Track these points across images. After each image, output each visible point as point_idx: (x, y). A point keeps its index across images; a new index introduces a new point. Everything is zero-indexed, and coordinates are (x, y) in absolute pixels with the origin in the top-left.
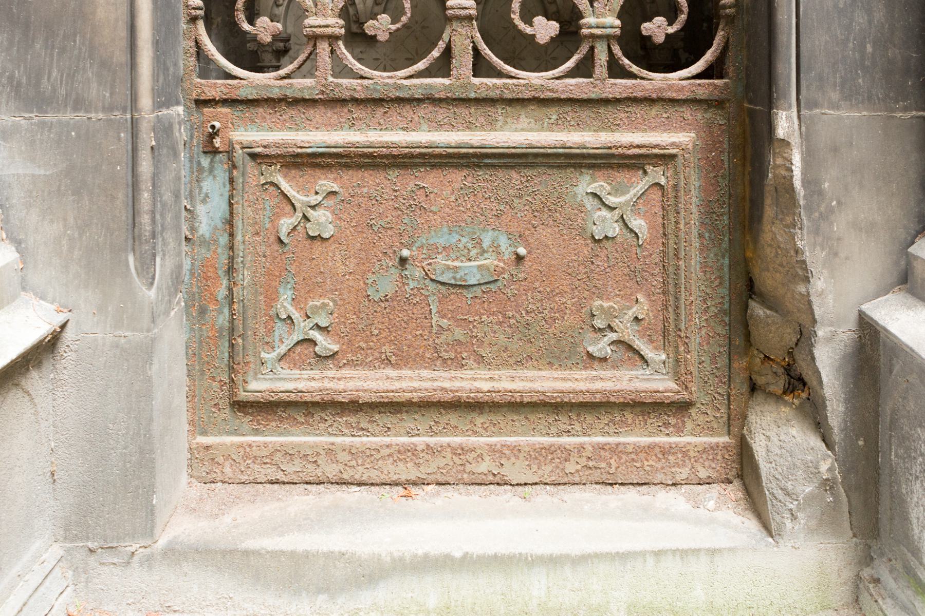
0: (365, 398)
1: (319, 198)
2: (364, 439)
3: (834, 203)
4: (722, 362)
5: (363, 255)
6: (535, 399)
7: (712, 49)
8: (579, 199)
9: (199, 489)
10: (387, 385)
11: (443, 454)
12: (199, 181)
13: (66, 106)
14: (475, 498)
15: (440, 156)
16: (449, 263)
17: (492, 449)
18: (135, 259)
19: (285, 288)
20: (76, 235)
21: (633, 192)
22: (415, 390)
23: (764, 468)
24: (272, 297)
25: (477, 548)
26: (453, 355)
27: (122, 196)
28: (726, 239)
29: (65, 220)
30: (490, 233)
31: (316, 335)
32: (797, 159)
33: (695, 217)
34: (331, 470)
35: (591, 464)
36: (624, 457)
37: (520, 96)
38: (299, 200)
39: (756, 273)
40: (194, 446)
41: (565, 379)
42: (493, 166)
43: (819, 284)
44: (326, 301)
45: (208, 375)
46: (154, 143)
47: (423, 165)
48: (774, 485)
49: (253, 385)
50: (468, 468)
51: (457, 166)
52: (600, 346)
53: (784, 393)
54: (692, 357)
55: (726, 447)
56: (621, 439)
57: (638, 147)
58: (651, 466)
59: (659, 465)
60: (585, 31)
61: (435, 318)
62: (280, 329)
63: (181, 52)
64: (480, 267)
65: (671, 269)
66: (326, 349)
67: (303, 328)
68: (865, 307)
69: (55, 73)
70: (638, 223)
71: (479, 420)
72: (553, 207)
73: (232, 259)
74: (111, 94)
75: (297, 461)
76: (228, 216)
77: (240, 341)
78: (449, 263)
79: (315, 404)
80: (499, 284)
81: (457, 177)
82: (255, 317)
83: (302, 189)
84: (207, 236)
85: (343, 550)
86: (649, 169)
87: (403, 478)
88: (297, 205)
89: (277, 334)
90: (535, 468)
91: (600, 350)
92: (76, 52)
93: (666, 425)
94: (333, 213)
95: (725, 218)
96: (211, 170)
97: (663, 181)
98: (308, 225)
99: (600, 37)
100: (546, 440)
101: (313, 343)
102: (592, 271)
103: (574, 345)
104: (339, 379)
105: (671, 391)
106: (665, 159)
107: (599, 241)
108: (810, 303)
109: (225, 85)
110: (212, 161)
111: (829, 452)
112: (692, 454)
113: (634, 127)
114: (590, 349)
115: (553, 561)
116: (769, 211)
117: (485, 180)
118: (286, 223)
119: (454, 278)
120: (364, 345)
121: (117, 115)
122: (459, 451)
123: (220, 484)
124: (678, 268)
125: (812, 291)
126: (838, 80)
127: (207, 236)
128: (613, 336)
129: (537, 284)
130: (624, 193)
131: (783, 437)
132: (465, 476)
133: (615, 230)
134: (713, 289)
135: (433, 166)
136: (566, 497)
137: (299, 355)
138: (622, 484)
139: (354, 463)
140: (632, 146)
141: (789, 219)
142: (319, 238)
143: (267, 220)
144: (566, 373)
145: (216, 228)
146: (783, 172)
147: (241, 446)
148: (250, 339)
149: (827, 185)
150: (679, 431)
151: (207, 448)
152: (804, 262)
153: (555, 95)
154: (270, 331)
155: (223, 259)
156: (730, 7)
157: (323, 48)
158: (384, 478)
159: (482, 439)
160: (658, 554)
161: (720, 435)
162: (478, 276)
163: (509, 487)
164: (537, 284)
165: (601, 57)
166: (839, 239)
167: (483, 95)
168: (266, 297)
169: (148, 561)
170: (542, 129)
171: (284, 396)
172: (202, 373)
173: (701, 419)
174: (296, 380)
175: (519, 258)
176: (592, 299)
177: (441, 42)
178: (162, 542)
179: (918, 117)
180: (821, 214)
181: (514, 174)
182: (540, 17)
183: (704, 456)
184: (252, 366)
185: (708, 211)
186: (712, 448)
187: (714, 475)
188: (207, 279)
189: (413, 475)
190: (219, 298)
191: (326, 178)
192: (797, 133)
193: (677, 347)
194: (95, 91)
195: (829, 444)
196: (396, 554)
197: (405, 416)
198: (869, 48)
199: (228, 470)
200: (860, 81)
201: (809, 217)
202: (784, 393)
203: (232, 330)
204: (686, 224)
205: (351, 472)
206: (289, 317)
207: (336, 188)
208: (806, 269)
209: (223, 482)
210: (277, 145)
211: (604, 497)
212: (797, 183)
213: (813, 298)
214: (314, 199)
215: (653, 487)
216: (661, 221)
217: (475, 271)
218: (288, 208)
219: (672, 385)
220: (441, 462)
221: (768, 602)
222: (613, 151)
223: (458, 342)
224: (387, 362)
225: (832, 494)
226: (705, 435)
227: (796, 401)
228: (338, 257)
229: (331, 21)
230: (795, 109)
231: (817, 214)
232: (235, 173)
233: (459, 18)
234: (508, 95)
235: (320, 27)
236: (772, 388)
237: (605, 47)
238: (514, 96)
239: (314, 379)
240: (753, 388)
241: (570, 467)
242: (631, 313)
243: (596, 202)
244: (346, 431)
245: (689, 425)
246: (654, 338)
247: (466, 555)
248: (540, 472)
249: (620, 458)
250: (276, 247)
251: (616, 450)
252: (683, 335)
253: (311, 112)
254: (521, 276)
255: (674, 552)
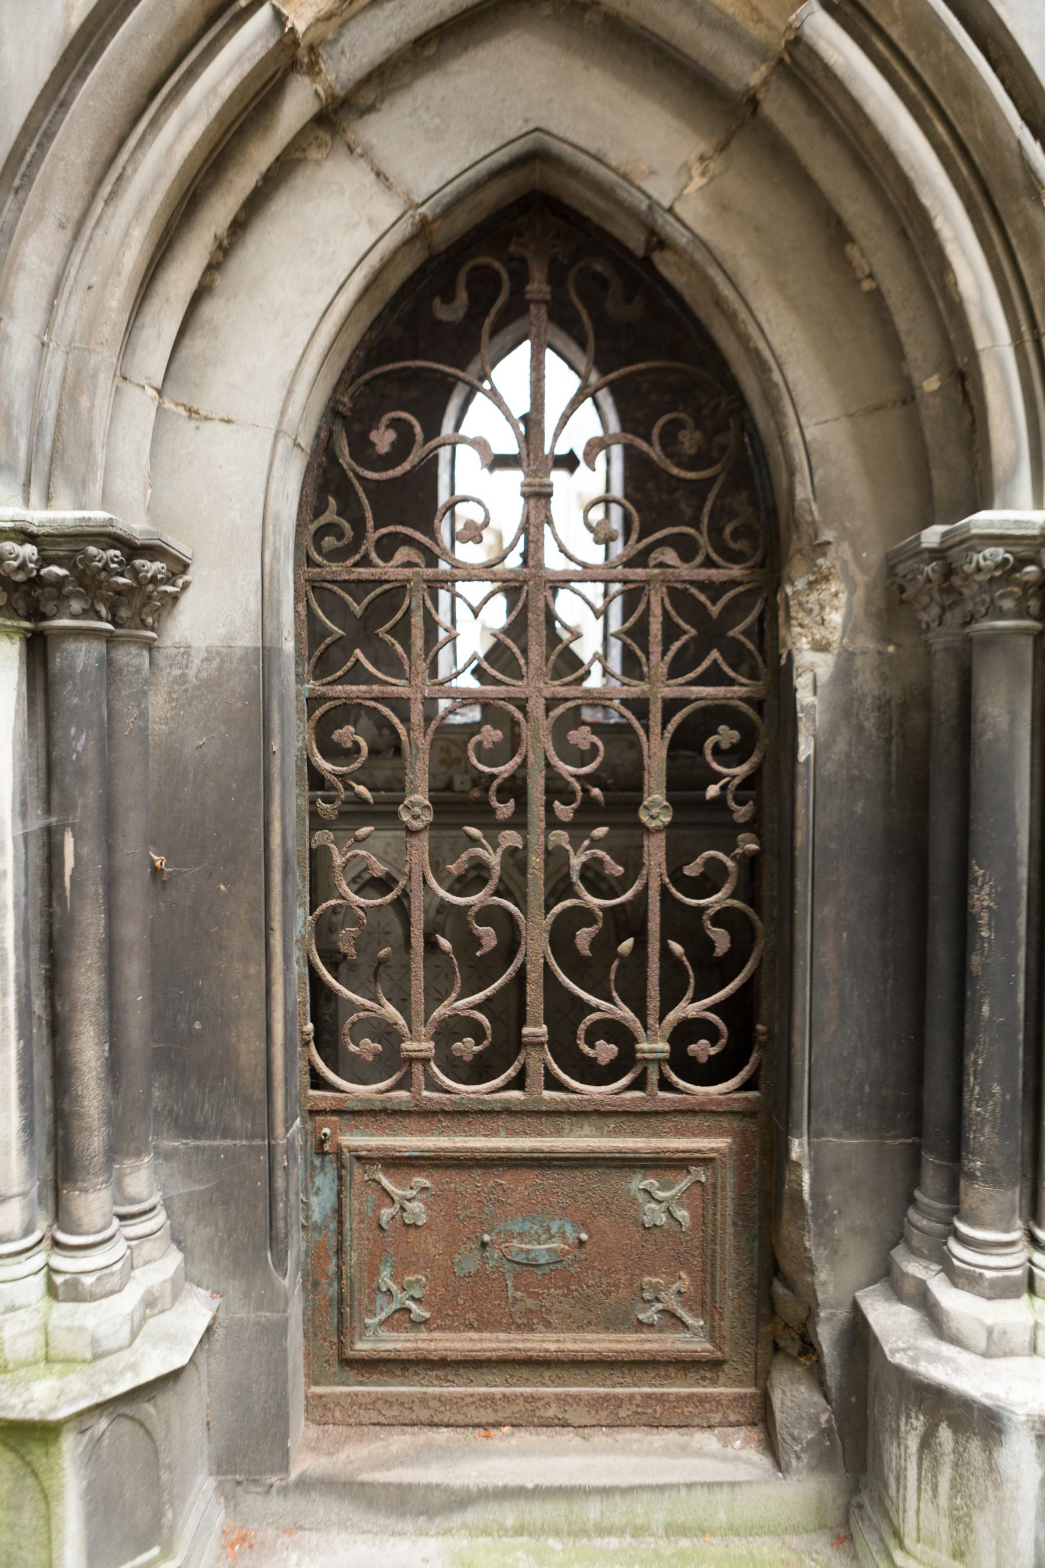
0: (452, 1356)
1: (414, 1193)
2: (451, 1389)
3: (836, 1212)
4: (751, 1326)
5: (451, 1239)
6: (594, 1358)
7: (747, 1068)
8: (632, 1194)
9: (314, 1431)
10: (468, 1346)
11: (517, 1401)
12: (312, 1177)
13: (216, 1134)
14: (544, 1438)
15: (516, 1159)
16: (523, 1246)
17: (558, 1398)
18: (272, 1256)
19: (385, 1266)
20: (225, 1236)
21: (678, 1187)
22: (494, 1350)
23: (778, 1415)
24: (375, 1273)
25: (545, 1481)
26: (525, 1321)
27: (262, 1206)
28: (756, 1226)
29: (216, 1224)
30: (558, 1222)
31: (413, 1306)
32: (806, 1177)
33: (730, 1210)
34: (424, 1415)
35: (640, 1410)
36: (667, 1405)
37: (584, 1109)
38: (397, 1195)
39: (778, 1256)
40: (309, 1395)
41: (619, 1341)
42: (561, 1167)
43: (822, 1275)
44: (420, 1277)
45: (320, 1336)
46: (286, 1164)
47: (502, 1166)
48: (784, 1432)
49: (359, 1346)
50: (538, 1413)
51: (530, 1167)
52: (648, 1314)
53: (800, 1354)
54: (726, 1324)
55: (753, 1396)
56: (665, 1390)
57: (683, 1152)
58: (690, 1412)
59: (696, 1412)
60: (639, 1055)
61: (511, 1291)
62: (381, 1299)
63: (298, 1071)
64: (548, 1250)
65: (709, 1252)
66: (419, 1316)
67: (401, 1298)
68: (857, 1294)
69: (207, 1107)
70: (682, 1214)
71: (547, 1374)
72: (609, 1201)
73: (340, 1243)
74: (253, 1125)
75: (395, 1408)
76: (336, 1206)
77: (348, 1310)
78: (523, 1246)
79: (410, 1362)
80: (565, 1263)
81: (532, 1177)
82: (360, 1290)
83: (399, 1185)
84: (319, 1222)
85: (439, 1482)
86: (693, 1169)
87: (484, 1421)
88: (396, 1198)
89: (378, 1304)
90: (593, 1413)
91: (648, 1318)
92: (223, 1091)
93: (704, 1378)
94: (425, 1204)
95: (756, 1208)
96: (322, 1168)
97: (703, 1179)
98: (405, 1215)
99: (652, 1060)
100: (602, 1390)
101: (409, 1311)
102: (643, 1253)
103: (627, 1313)
104: (431, 1341)
105: (707, 1351)
106: (705, 1161)
107: (649, 1228)
108: (814, 1291)
109: (333, 1098)
110: (323, 1161)
111: (829, 1407)
112: (724, 1402)
113: (680, 1133)
114: (640, 1317)
115: (605, 1492)
116: (786, 1214)
117: (554, 1179)
118: (386, 1213)
119: (527, 1259)
120: (451, 1313)
121: (258, 1142)
122: (530, 1400)
123: (331, 1426)
124: (714, 1251)
125: (816, 1281)
126: (841, 1114)
127: (319, 1222)
128: (660, 1306)
129: (596, 1264)
130: (670, 1189)
131: (794, 1393)
132: (535, 1420)
133: (663, 1219)
134: (745, 1267)
135: (510, 1167)
136: (618, 1438)
137: (397, 1320)
138: (666, 1426)
139: (443, 1409)
140: (677, 1151)
141: (800, 1223)
142: (415, 1226)
143: (370, 1210)
144: (619, 1336)
145: (326, 1216)
146: (796, 1186)
147: (348, 1395)
148: (356, 1308)
149: (830, 1197)
150: (714, 1383)
151: (320, 1397)
152: (810, 1258)
153: (613, 1109)
154: (372, 1301)
155: (333, 1242)
156: (763, 1035)
157: (418, 1069)
158: (467, 1421)
159: (550, 1390)
160: (690, 1486)
161: (749, 1387)
162: (547, 1257)
163: (572, 1429)
164: (596, 1264)
165: (653, 1077)
166: (839, 1240)
167: (552, 1109)
168: (369, 1273)
169: (284, 1491)
170: (602, 1136)
171: (384, 1355)
172: (315, 1335)
173: (733, 1374)
174: (395, 1341)
175: (581, 1243)
176: (641, 1275)
177: (516, 1063)
178: (294, 1475)
179: (905, 1144)
180: (825, 1220)
181: (577, 1173)
182: (602, 1041)
183: (735, 1404)
184: (358, 1329)
185: (741, 1202)
186: (741, 1397)
187: (742, 1419)
188: (319, 1258)
189: (492, 1418)
190: (330, 1274)
191: (420, 1176)
192: (806, 1157)
193: (713, 1316)
194: (238, 1122)
195: (828, 1401)
196: (481, 1486)
197: (485, 1371)
198: (867, 1089)
199: (338, 1414)
200: (859, 1115)
201: (815, 1224)
202: (800, 1354)
203: (341, 1300)
204: (722, 1215)
205: (440, 1416)
206: (389, 1290)
207: (427, 1183)
208: (811, 1264)
209: (334, 1424)
210: (378, 1149)
211: (650, 1438)
212: (806, 1196)
213: (817, 1287)
214: (409, 1193)
215: (691, 1429)
216: (700, 1211)
217: (544, 1252)
218: (387, 1200)
219: (708, 1346)
220: (516, 1409)
221: (777, 1523)
222: (662, 1155)
223: (530, 1311)
224: (471, 1327)
225: (830, 1440)
226: (737, 1387)
227: (808, 1363)
228: (430, 1240)
229: (424, 1045)
230: (805, 1138)
231: (821, 1221)
232: (344, 1172)
233: (534, 1045)
234: (573, 1108)
235: (415, 1051)
236: (789, 1351)
237: (656, 1068)
238: (579, 1109)
239: (409, 1340)
240: (776, 1348)
241: (623, 1413)
242: (674, 1287)
243: (646, 1196)
244: (435, 1382)
245: (723, 1378)
246: (694, 1307)
247: (536, 1487)
248: (598, 1417)
249: (664, 1405)
250: (377, 1232)
251: (661, 1399)
252: (717, 1305)
253: (407, 1122)
254: (583, 1257)
255: (703, 1484)
